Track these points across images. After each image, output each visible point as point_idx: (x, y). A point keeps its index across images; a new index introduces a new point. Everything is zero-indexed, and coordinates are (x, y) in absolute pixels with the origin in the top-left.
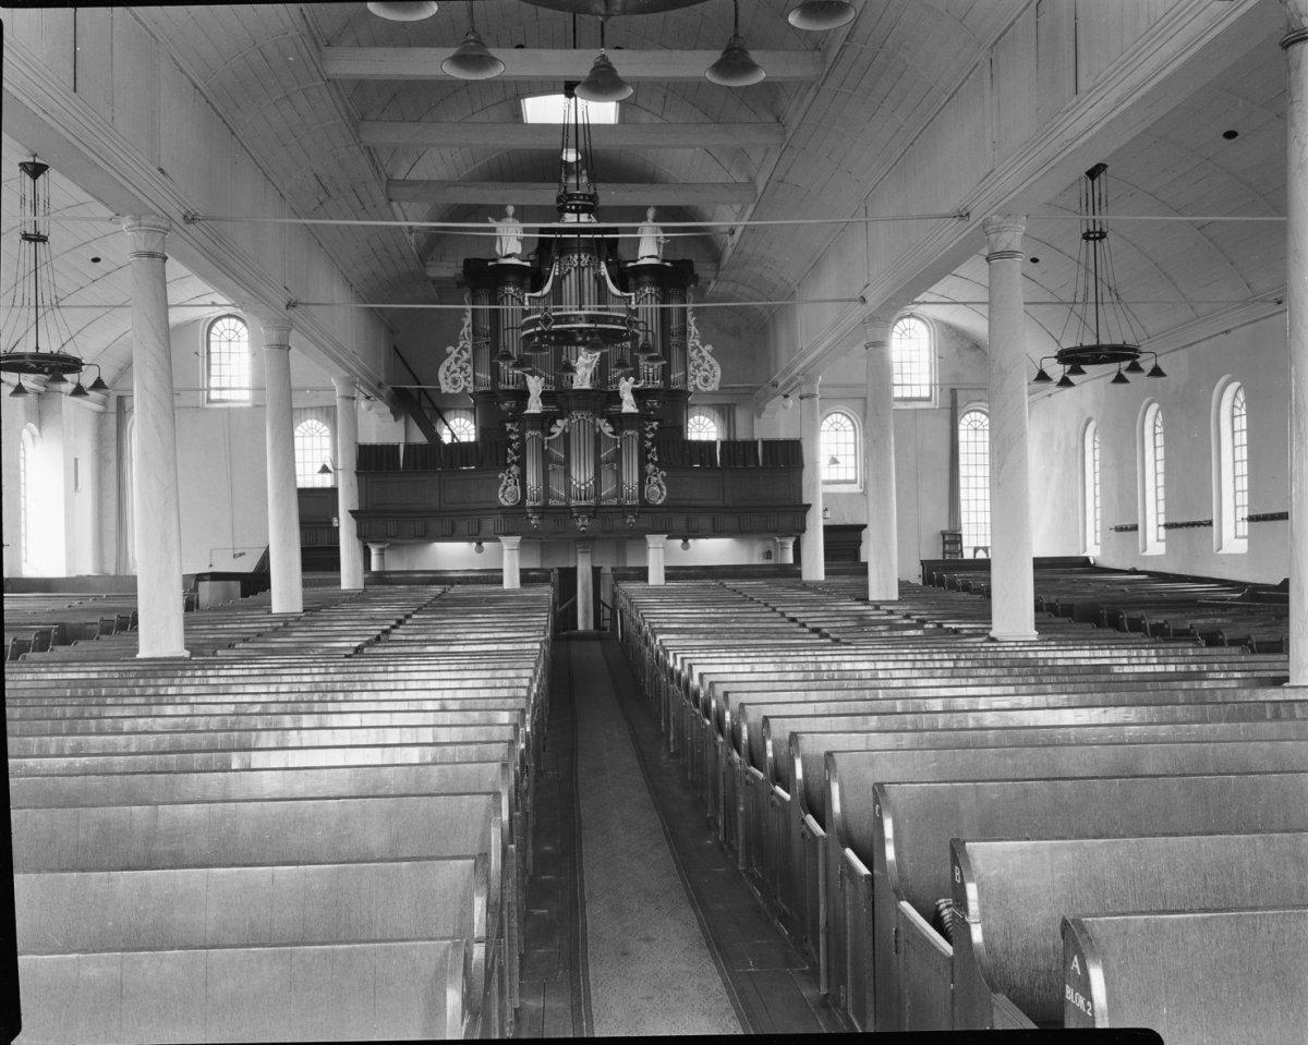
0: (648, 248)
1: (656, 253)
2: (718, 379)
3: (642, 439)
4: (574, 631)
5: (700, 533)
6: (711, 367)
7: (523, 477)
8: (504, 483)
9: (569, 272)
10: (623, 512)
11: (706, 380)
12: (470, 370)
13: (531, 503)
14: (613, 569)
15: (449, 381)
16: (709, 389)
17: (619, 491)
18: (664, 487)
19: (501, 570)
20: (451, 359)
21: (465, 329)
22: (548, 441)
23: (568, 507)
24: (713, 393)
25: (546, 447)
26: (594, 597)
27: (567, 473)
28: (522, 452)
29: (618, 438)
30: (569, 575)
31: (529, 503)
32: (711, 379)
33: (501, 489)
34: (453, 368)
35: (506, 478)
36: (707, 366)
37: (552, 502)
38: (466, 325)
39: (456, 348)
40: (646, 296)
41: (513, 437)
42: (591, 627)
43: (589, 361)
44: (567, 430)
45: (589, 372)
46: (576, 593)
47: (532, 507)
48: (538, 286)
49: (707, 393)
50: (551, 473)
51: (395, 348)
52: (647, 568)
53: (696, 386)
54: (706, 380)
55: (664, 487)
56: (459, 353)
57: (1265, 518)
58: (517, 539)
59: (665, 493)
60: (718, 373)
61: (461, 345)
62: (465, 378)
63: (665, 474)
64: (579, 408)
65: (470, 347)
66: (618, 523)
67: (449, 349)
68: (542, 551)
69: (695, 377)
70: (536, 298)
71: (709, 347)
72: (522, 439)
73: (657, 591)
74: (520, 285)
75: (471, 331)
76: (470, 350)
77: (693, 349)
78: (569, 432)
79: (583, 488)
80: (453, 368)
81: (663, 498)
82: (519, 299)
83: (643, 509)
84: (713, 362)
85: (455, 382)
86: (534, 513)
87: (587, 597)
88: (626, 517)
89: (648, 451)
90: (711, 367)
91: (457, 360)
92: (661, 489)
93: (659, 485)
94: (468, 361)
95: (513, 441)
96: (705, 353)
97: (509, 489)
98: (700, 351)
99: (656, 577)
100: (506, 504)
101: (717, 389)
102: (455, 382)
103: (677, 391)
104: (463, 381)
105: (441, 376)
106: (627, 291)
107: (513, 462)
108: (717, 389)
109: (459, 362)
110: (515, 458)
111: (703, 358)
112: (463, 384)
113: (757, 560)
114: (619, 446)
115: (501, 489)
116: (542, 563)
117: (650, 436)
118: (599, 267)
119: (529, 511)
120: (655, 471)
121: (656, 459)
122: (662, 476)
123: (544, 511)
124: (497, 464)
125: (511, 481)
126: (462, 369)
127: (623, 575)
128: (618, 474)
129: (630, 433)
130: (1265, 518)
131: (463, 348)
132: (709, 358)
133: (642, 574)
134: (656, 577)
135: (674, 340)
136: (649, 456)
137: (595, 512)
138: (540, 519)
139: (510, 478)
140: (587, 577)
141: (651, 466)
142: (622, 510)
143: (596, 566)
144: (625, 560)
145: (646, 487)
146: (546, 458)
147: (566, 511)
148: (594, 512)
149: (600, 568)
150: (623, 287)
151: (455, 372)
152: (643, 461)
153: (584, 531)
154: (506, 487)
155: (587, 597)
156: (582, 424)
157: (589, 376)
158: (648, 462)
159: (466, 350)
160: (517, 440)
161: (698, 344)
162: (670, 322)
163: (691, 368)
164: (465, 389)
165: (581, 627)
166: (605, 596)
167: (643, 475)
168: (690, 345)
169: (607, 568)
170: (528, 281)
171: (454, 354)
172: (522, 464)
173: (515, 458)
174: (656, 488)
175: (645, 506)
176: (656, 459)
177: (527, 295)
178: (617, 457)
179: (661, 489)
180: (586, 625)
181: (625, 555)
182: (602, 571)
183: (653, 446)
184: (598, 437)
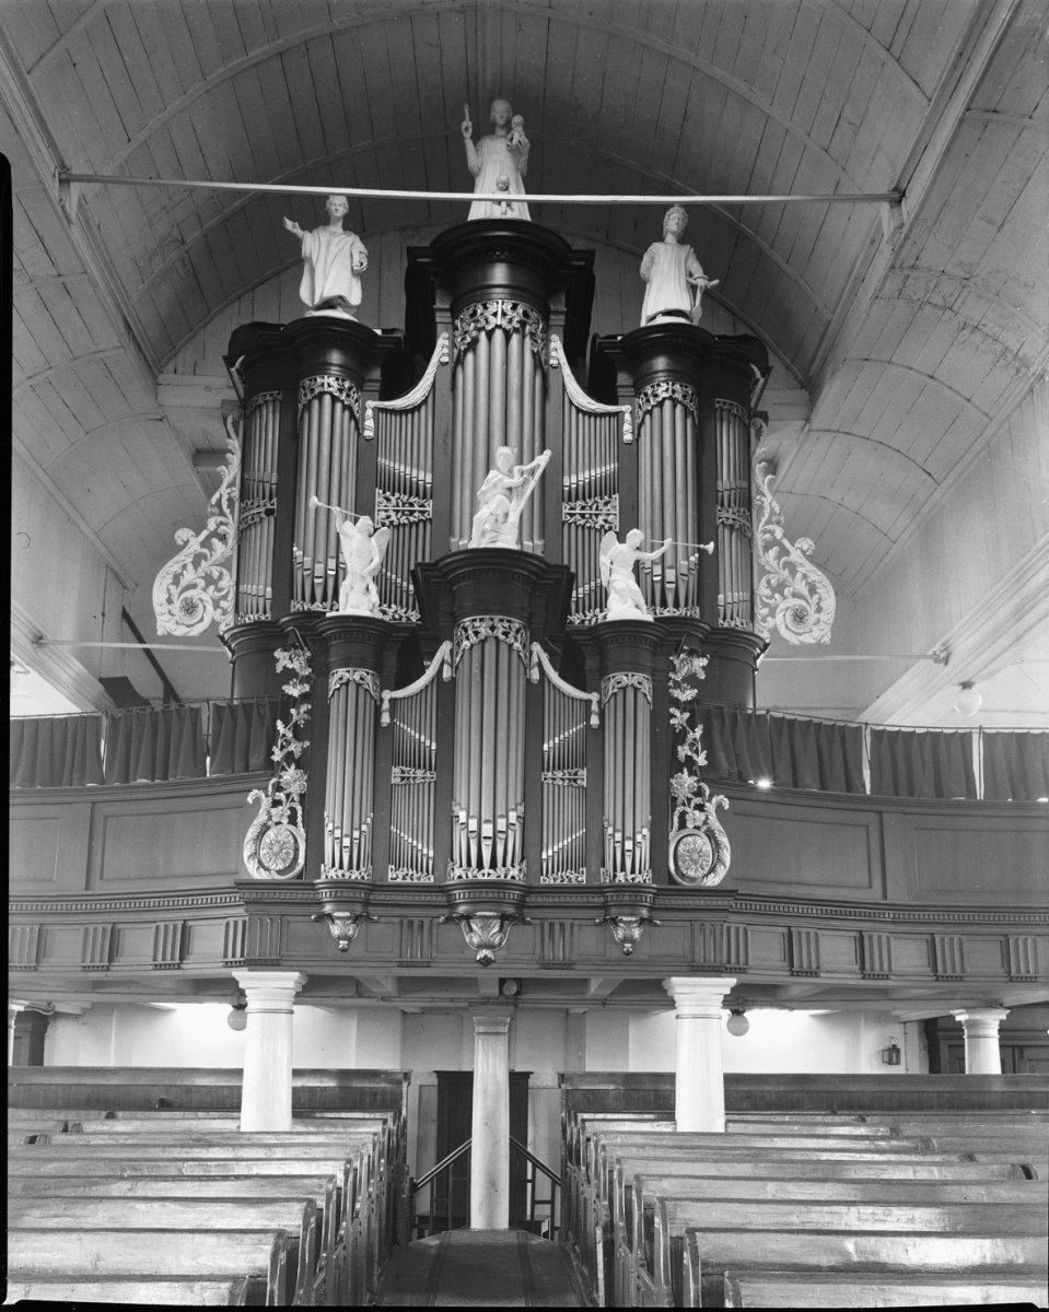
0: (668, 288)
1: (685, 305)
2: (828, 616)
3: (663, 701)
4: (457, 1237)
5: (782, 995)
6: (813, 590)
7: (311, 807)
8: (262, 818)
9: (475, 341)
10: (605, 907)
11: (799, 617)
12: (228, 582)
13: (333, 874)
14: (562, 1078)
15: (177, 604)
16: (809, 639)
17: (591, 850)
18: (724, 840)
19: (239, 1073)
20: (185, 557)
21: (223, 491)
22: (393, 701)
23: (443, 890)
24: (819, 648)
25: (386, 719)
26: (512, 1145)
27: (444, 793)
28: (315, 731)
29: (594, 697)
30: (455, 1089)
31: (329, 872)
32: (812, 617)
33: (252, 832)
34: (189, 576)
35: (266, 802)
36: (803, 588)
37: (395, 875)
38: (227, 480)
39: (198, 533)
40: (661, 404)
41: (293, 690)
42: (503, 1222)
43: (517, 480)
44: (447, 673)
45: (517, 507)
46: (469, 1134)
47: (335, 885)
48: (398, 383)
49: (804, 649)
50: (399, 794)
51: (125, 615)
52: (670, 1078)
53: (774, 631)
54: (799, 617)
55: (724, 840)
56: (206, 543)
57: (1014, 1068)
58: (289, 980)
59: (727, 856)
60: (830, 602)
61: (212, 524)
62: (216, 605)
63: (726, 804)
64: (483, 608)
65: (231, 531)
66: (587, 940)
67: (183, 534)
68: (404, 1040)
69: (772, 614)
70: (394, 412)
71: (806, 544)
72: (317, 696)
73: (697, 1146)
74: (355, 374)
75: (236, 492)
76: (232, 541)
77: (767, 548)
78: (453, 680)
79: (487, 830)
80: (189, 576)
81: (722, 872)
82: (349, 408)
83: (663, 901)
84: (816, 575)
85: (190, 608)
86: (339, 902)
87: (496, 1144)
88: (615, 921)
89: (680, 737)
90: (813, 590)
91: (197, 560)
92: (717, 846)
93: (710, 834)
94: (226, 564)
95: (294, 702)
96: (795, 556)
97: (271, 834)
98: (784, 552)
99: (699, 1107)
100: (259, 875)
101: (827, 639)
102: (190, 608)
103: (732, 630)
104: (210, 608)
105: (159, 595)
106: (615, 403)
107: (289, 758)
108: (827, 639)
109: (204, 563)
110: (296, 748)
111: (792, 567)
112: (210, 614)
113: (866, 1062)
114: (595, 721)
115: (252, 832)
116: (402, 1064)
117: (688, 694)
118: (547, 341)
119: (325, 895)
120: (699, 793)
121: (701, 760)
122: (719, 807)
123: (366, 899)
124: (247, 769)
125: (281, 813)
126: (209, 580)
127: (583, 1098)
128: (593, 799)
129: (625, 679)
130: (1014, 1068)
131: (214, 534)
132: (807, 567)
133: (654, 1095)
134: (699, 1107)
135: (726, 515)
136: (683, 751)
137: (521, 905)
138: (356, 919)
139: (276, 803)
140: (497, 1095)
141: (685, 782)
142: (606, 902)
143: (519, 1069)
144: (582, 1059)
145: (673, 836)
146: (385, 747)
147: (438, 903)
148: (520, 904)
149: (527, 1075)
150: (601, 388)
151: (194, 586)
152: (666, 763)
153: (486, 962)
154: (265, 828)
155: (496, 1144)
156: (490, 647)
157: (514, 518)
158: (676, 766)
159: (223, 538)
160: (305, 697)
161: (779, 533)
162: (715, 477)
163: (762, 590)
164: (214, 624)
165: (477, 1221)
166: (540, 1141)
167: (663, 807)
168: (760, 538)
169: (545, 1076)
170: (376, 374)
171: (195, 545)
172: (313, 765)
173: (296, 748)
174: (703, 843)
175: (669, 894)
176: (701, 760)
177: (371, 404)
178: (590, 751)
179: (717, 846)
180: (491, 1214)
181: (582, 1047)
182: (531, 1082)
183: (692, 724)
184: (535, 694)
